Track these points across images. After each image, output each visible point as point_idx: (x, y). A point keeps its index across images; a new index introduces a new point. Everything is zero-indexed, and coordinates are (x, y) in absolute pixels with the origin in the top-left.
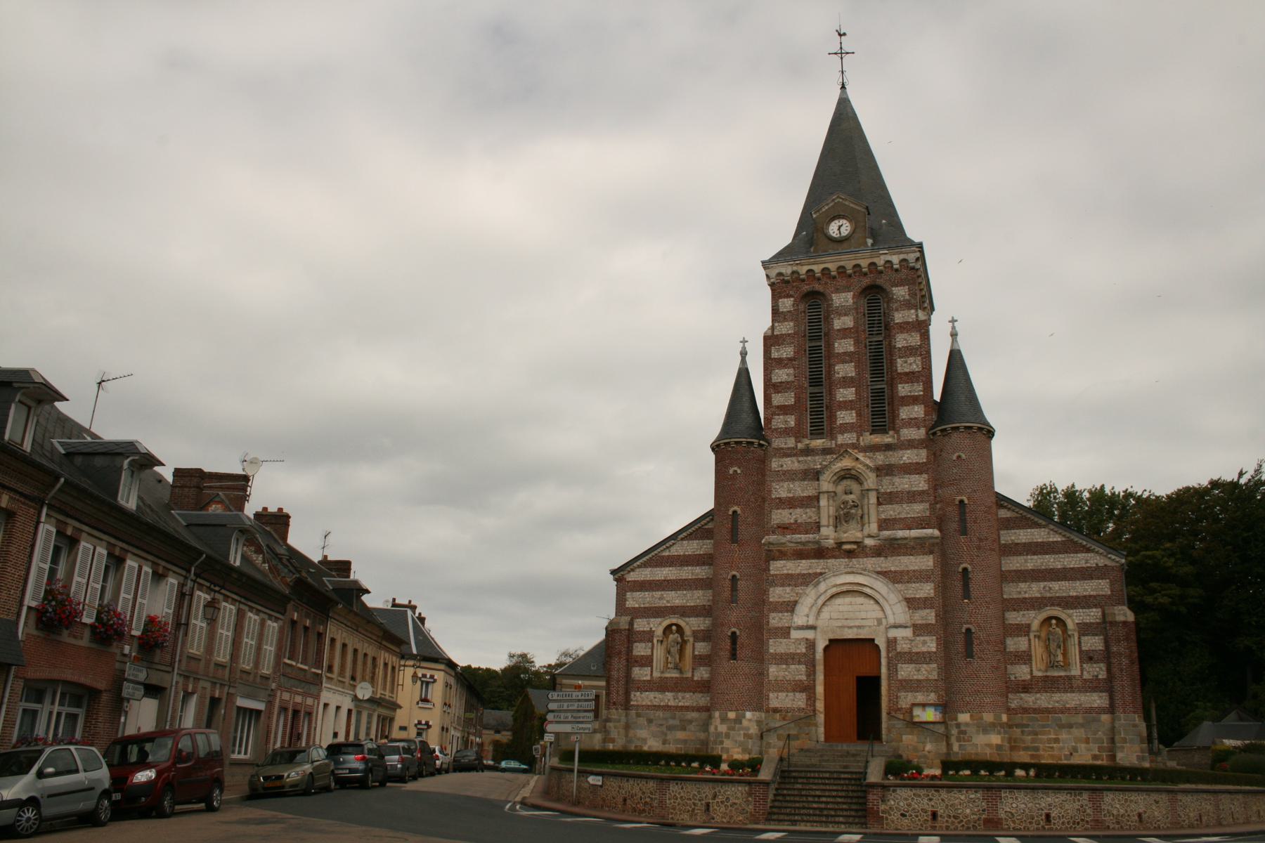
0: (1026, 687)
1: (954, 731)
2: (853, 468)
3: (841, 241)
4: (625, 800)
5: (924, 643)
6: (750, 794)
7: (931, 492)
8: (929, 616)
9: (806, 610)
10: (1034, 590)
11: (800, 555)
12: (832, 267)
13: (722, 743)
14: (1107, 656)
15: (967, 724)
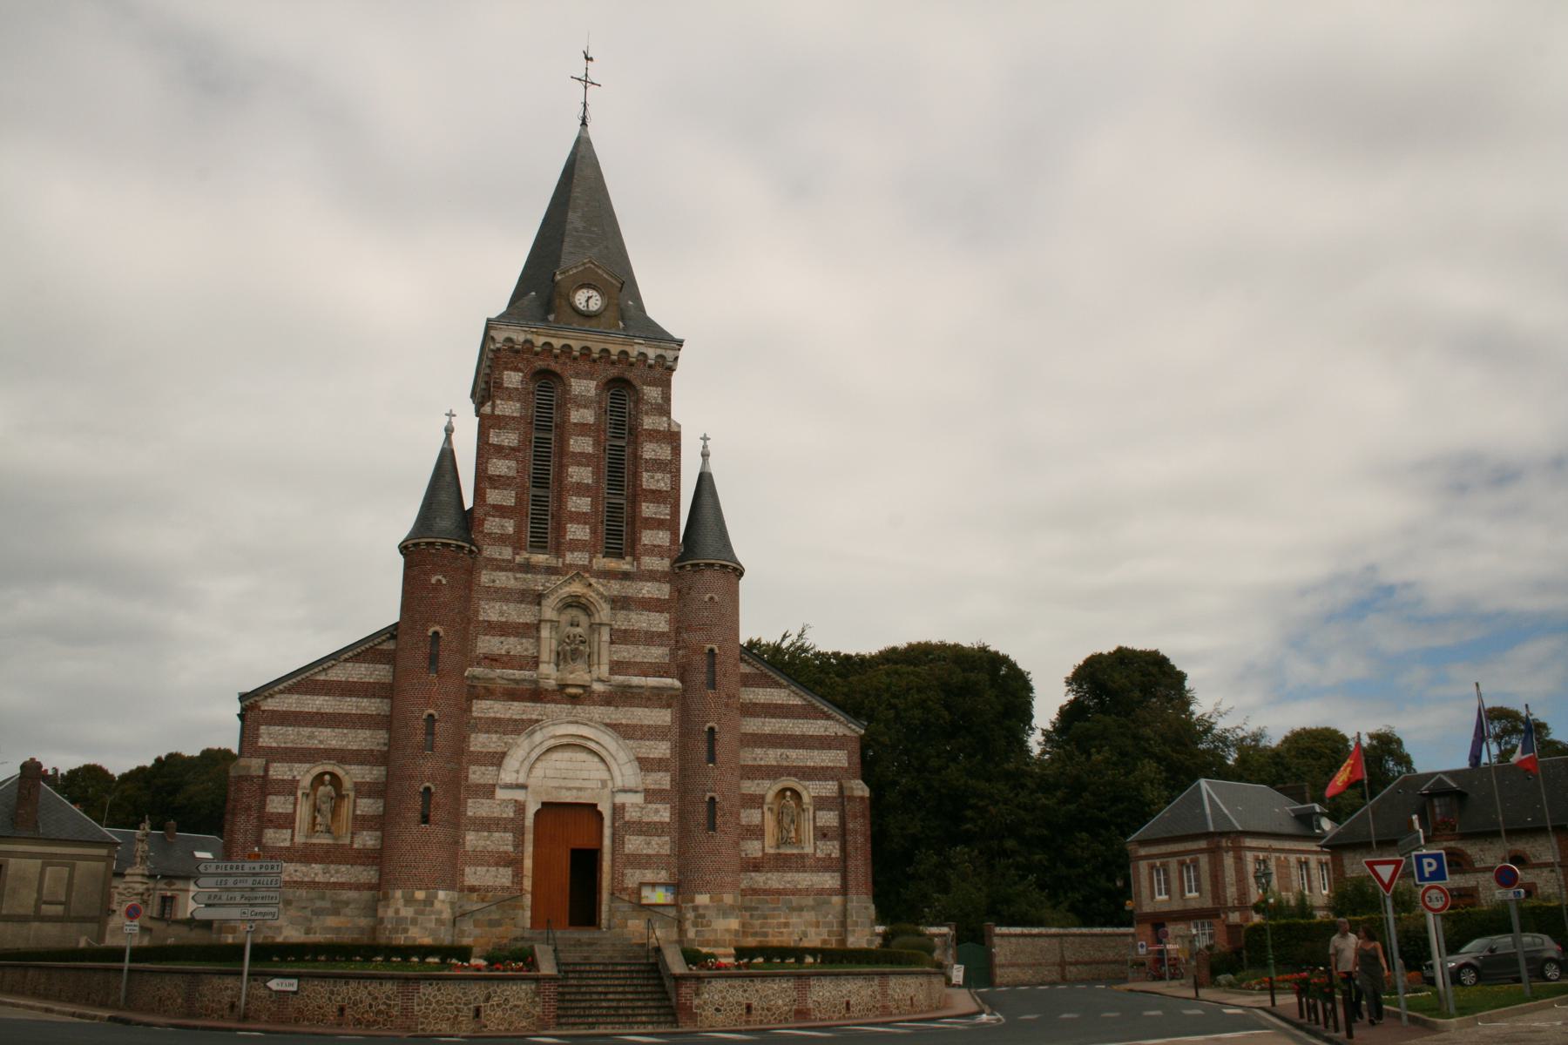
0: (756, 866)
1: (690, 915)
2: (583, 596)
3: (587, 316)
4: (342, 1009)
5: (657, 811)
6: (537, 994)
7: (673, 635)
8: (663, 780)
9: (517, 765)
10: (771, 757)
11: (512, 695)
12: (576, 346)
13: (406, 931)
14: (843, 833)
15: (706, 907)
